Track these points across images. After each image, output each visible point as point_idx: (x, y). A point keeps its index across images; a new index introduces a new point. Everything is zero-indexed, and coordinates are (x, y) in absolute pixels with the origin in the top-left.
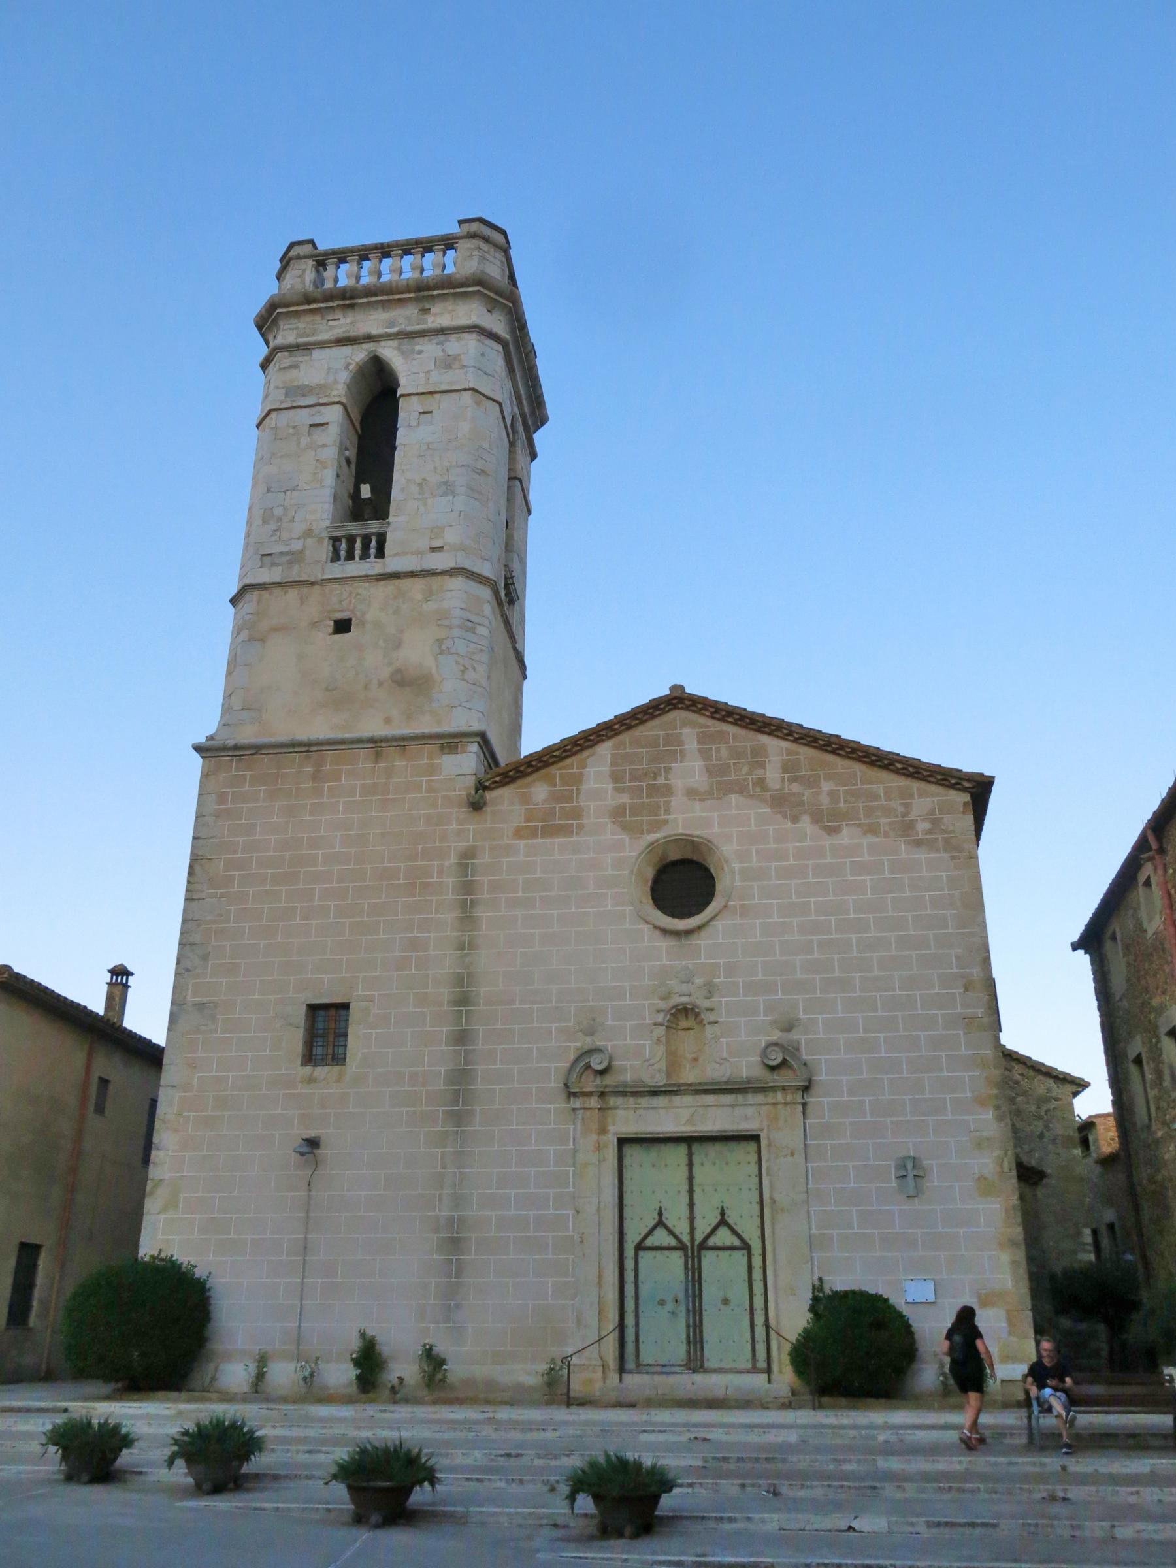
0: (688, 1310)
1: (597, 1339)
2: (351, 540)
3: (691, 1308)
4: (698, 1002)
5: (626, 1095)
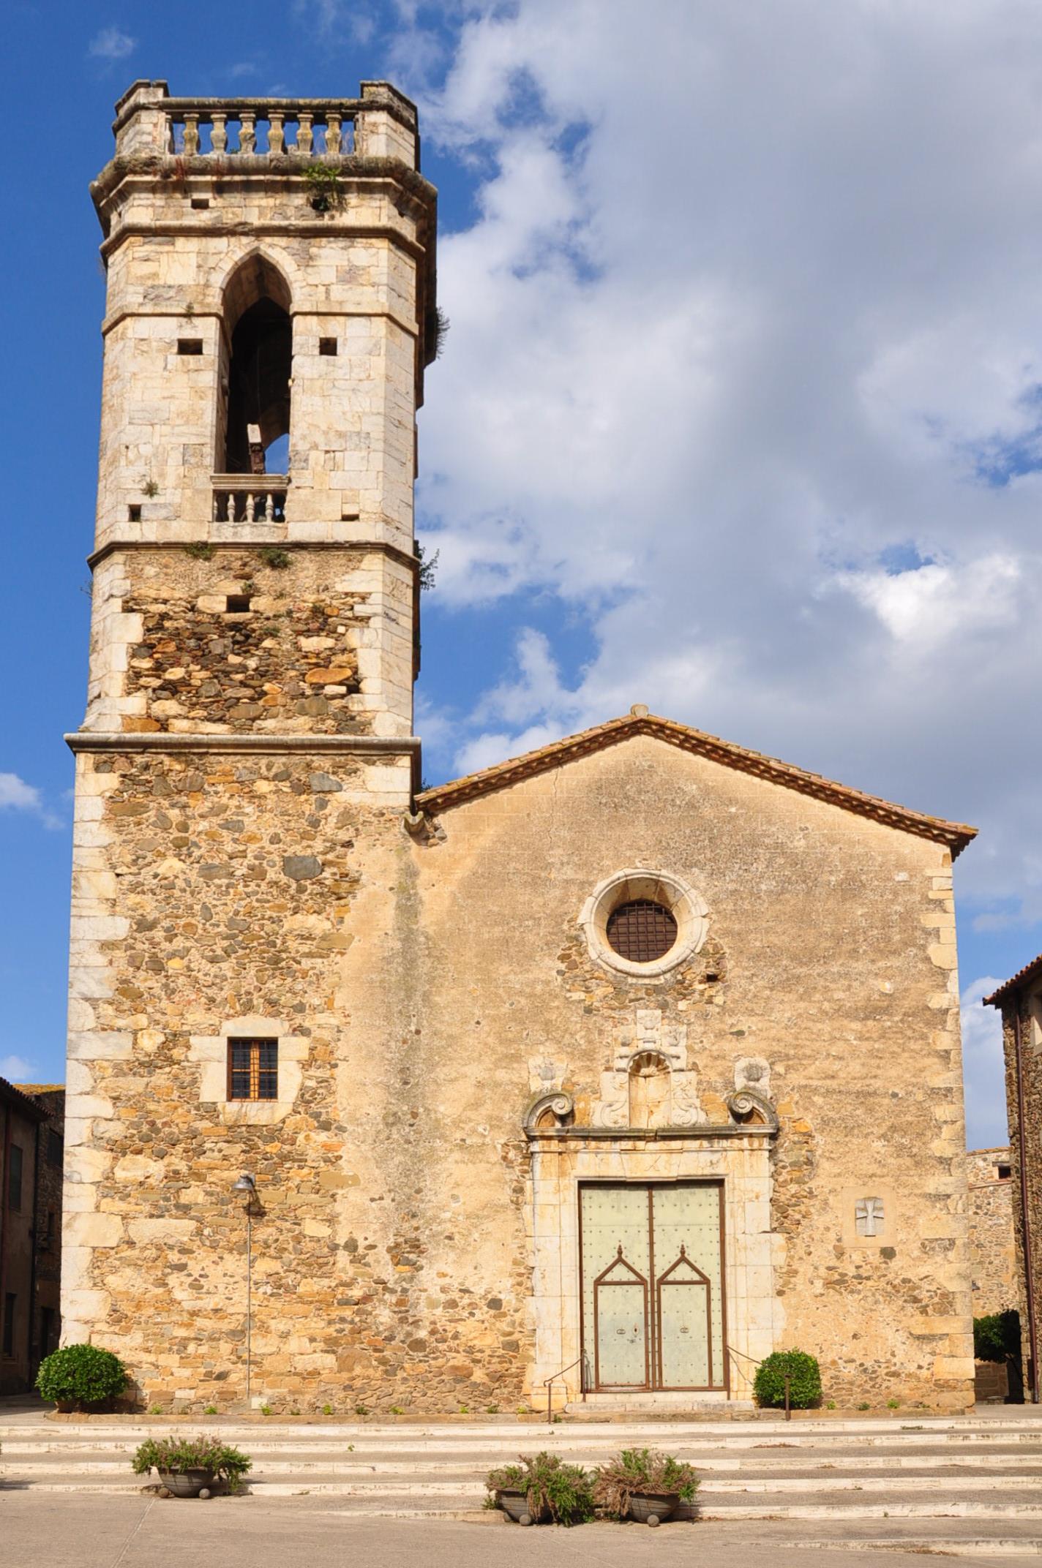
2: (241, 497)
4: (664, 1049)
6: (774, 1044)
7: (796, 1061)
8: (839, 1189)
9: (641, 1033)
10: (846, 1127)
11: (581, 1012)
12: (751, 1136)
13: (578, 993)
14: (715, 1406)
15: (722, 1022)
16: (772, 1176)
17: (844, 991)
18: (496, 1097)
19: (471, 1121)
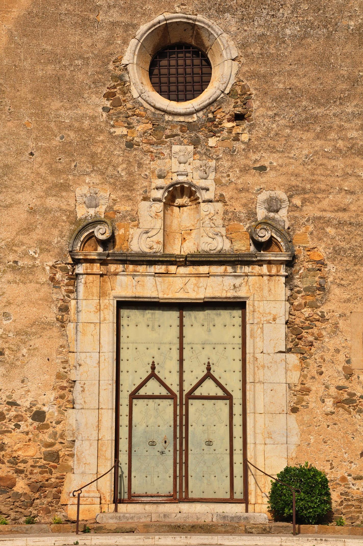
1: (96, 478)
4: (195, 182)
6: (292, 178)
7: (312, 195)
8: (348, 314)
9: (176, 167)
10: (355, 257)
11: (123, 146)
12: (269, 262)
13: (121, 129)
14: (232, 518)
15: (247, 157)
16: (288, 300)
17: (357, 130)
18: (46, 223)
19: (23, 244)
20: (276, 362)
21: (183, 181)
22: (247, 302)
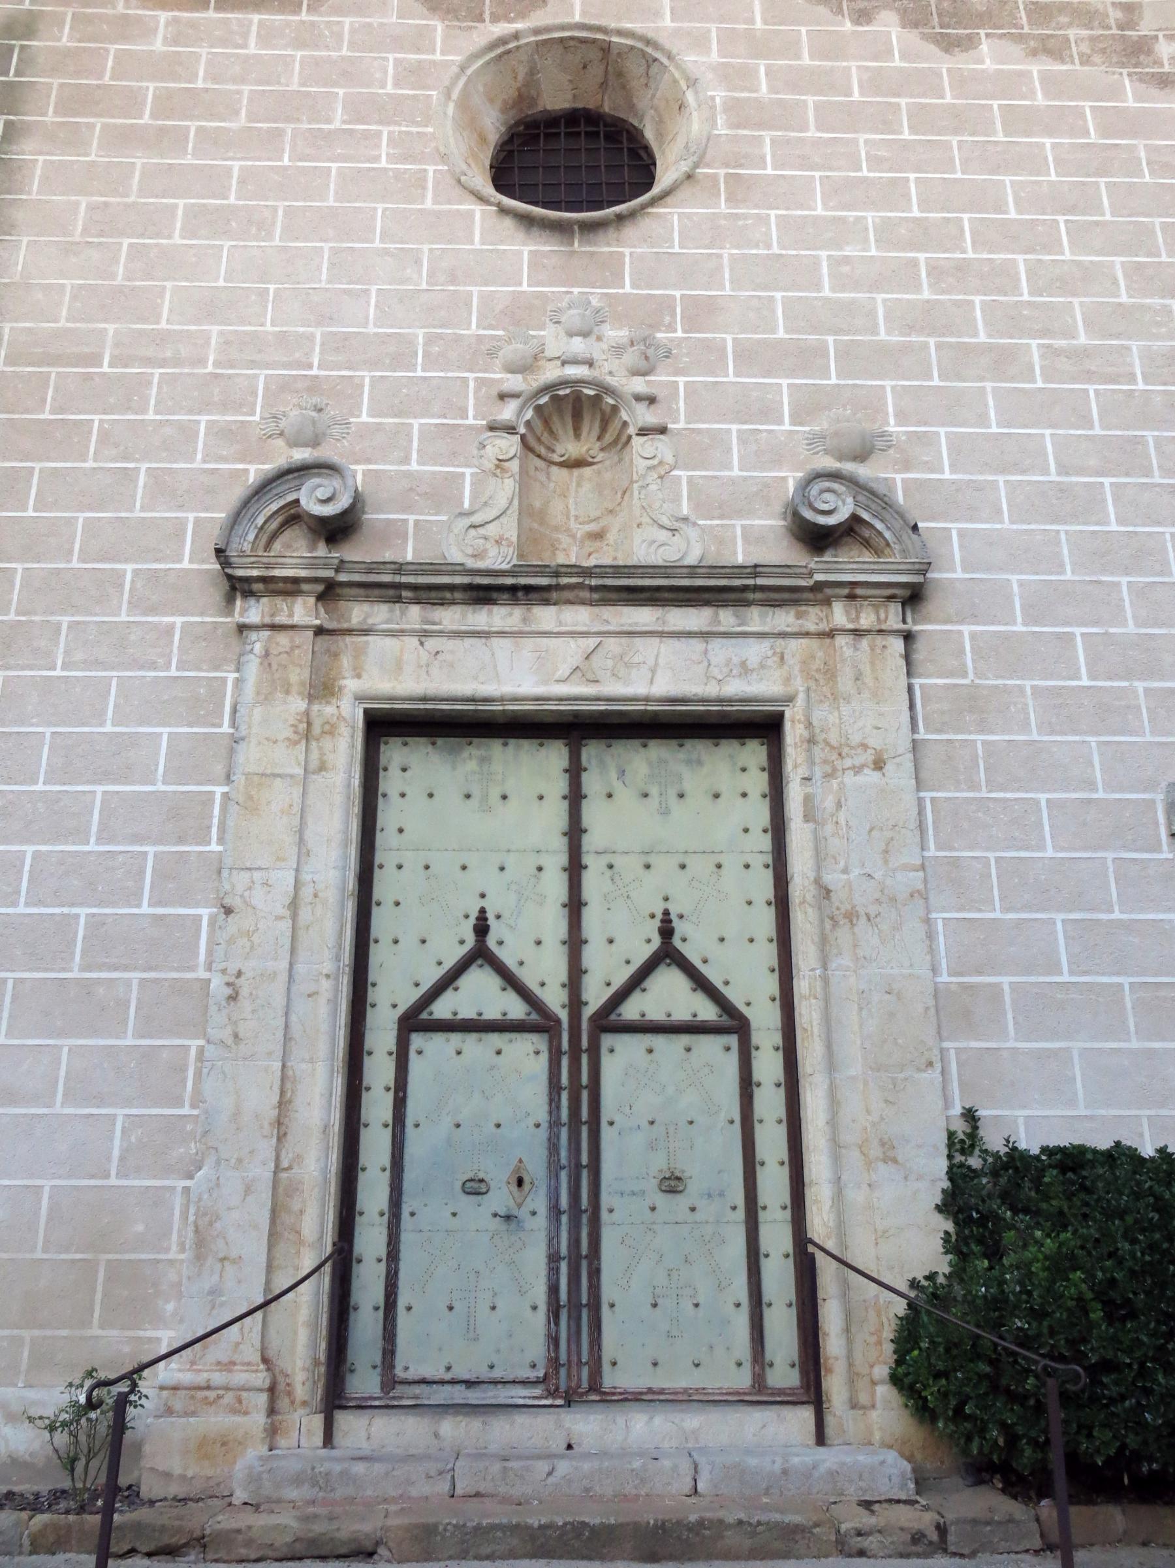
0: (555, 1211)
1: (260, 1300)
3: (564, 1202)
5: (398, 600)
20: (893, 900)
21: (579, 377)
22: (787, 715)
